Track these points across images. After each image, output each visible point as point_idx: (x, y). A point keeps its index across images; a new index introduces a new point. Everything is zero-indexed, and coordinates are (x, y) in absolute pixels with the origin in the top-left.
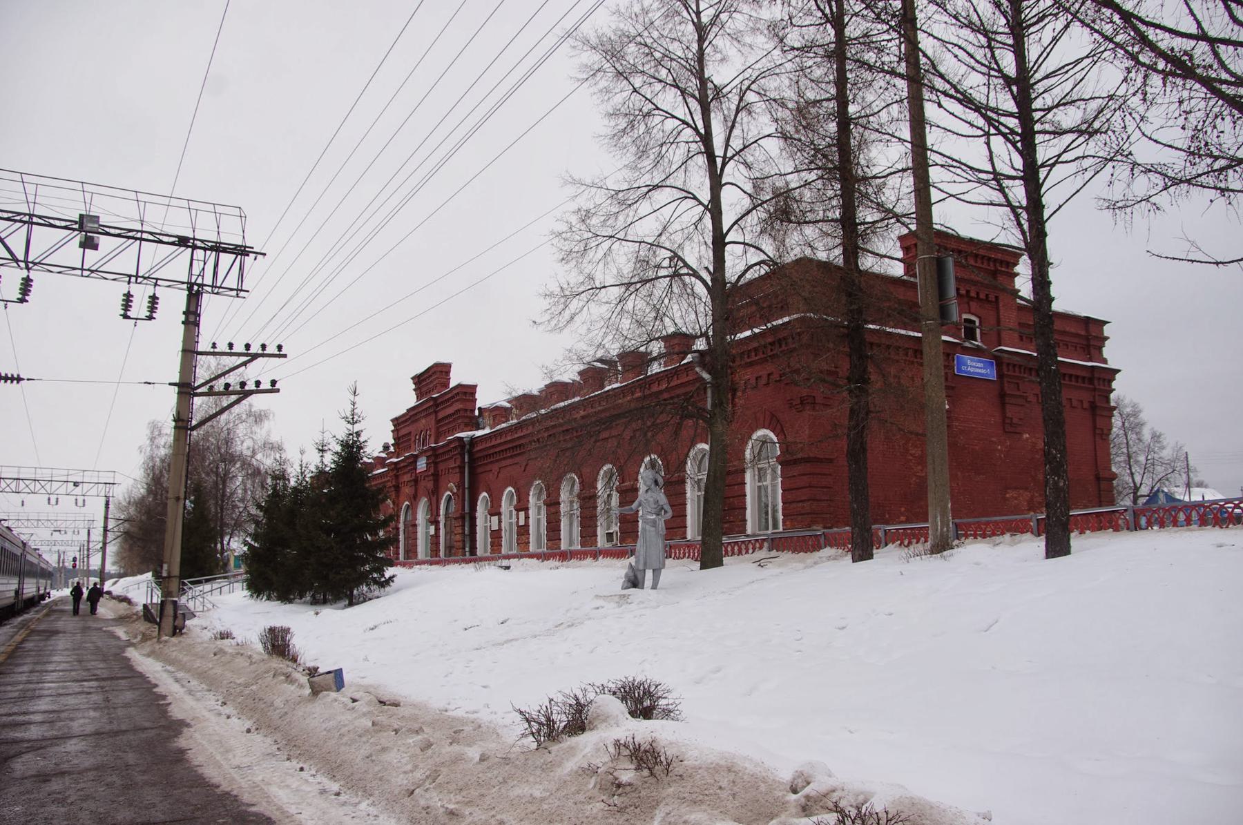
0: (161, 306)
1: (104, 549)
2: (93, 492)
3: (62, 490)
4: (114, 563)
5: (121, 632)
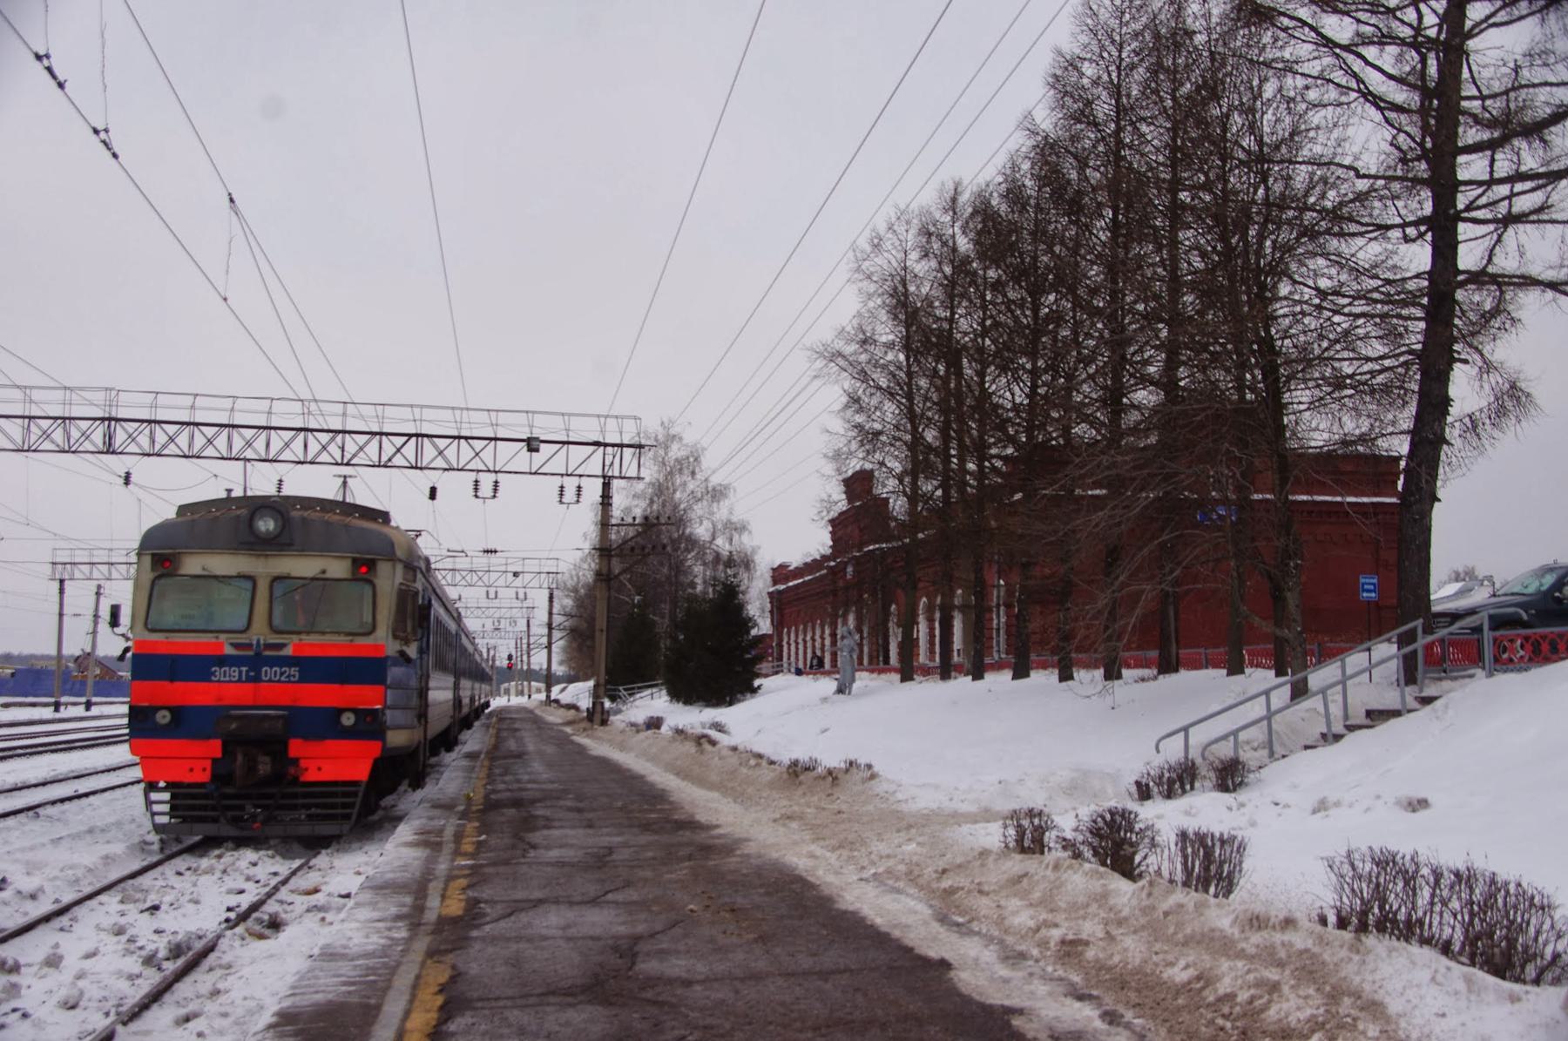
0: (584, 492)
1: (549, 647)
2: (535, 583)
3: (501, 582)
4: (561, 663)
5: (568, 730)
